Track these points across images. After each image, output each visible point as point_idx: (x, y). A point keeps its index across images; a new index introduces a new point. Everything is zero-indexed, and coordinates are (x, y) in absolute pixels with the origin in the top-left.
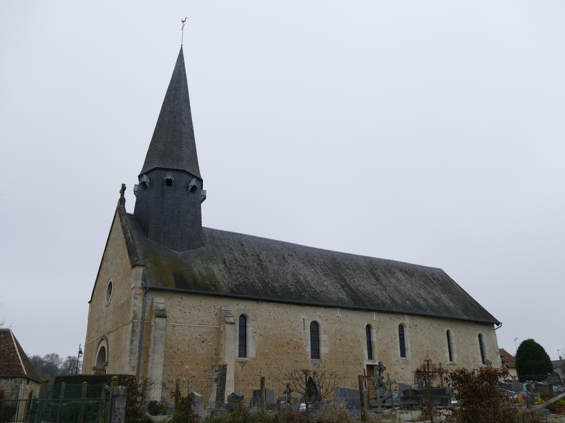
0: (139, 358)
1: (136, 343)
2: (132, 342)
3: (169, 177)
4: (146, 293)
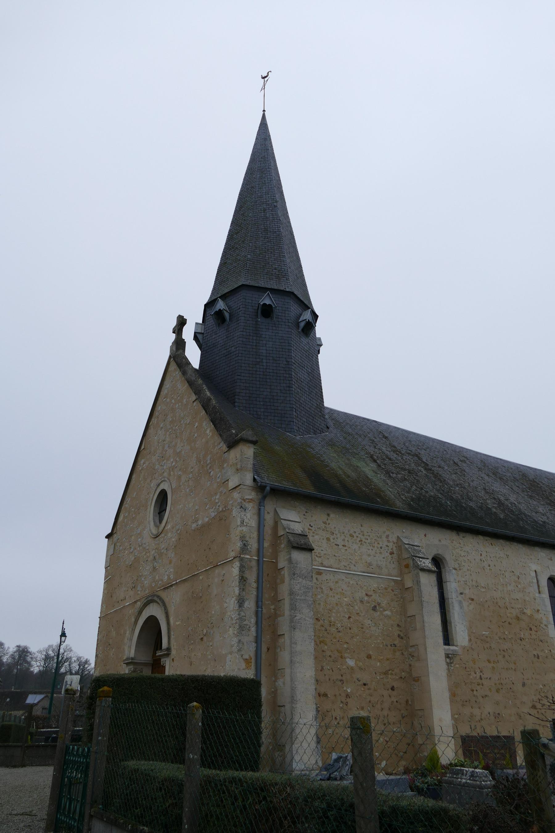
0: (258, 640)
1: (250, 604)
2: (241, 602)
3: (268, 302)
4: (264, 498)
